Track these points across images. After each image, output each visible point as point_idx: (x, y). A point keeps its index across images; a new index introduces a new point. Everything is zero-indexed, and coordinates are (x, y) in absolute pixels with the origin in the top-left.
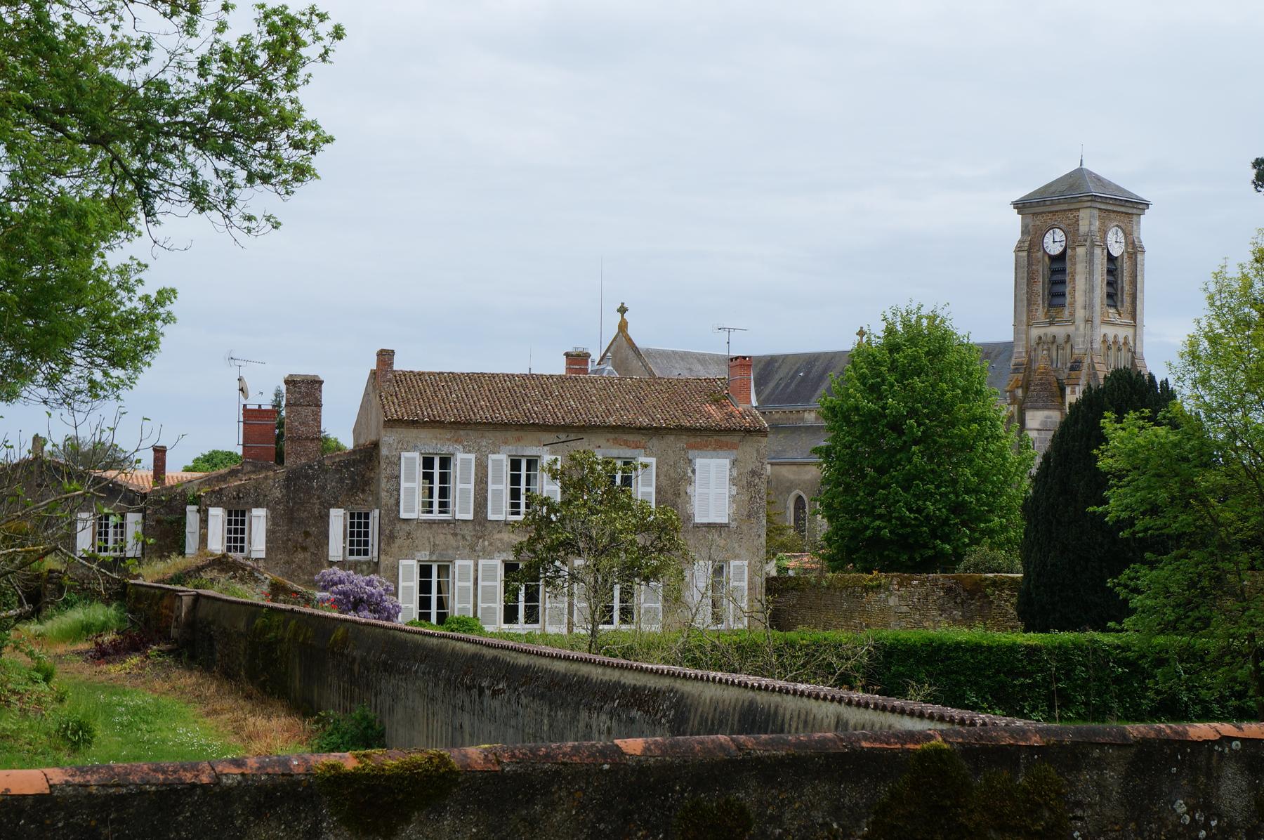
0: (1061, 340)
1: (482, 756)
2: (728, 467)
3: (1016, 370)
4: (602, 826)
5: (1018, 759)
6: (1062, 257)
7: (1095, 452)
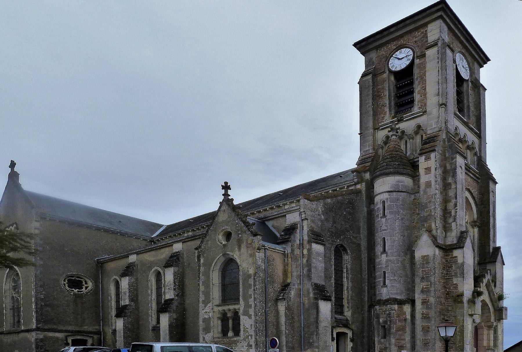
6: (408, 71)
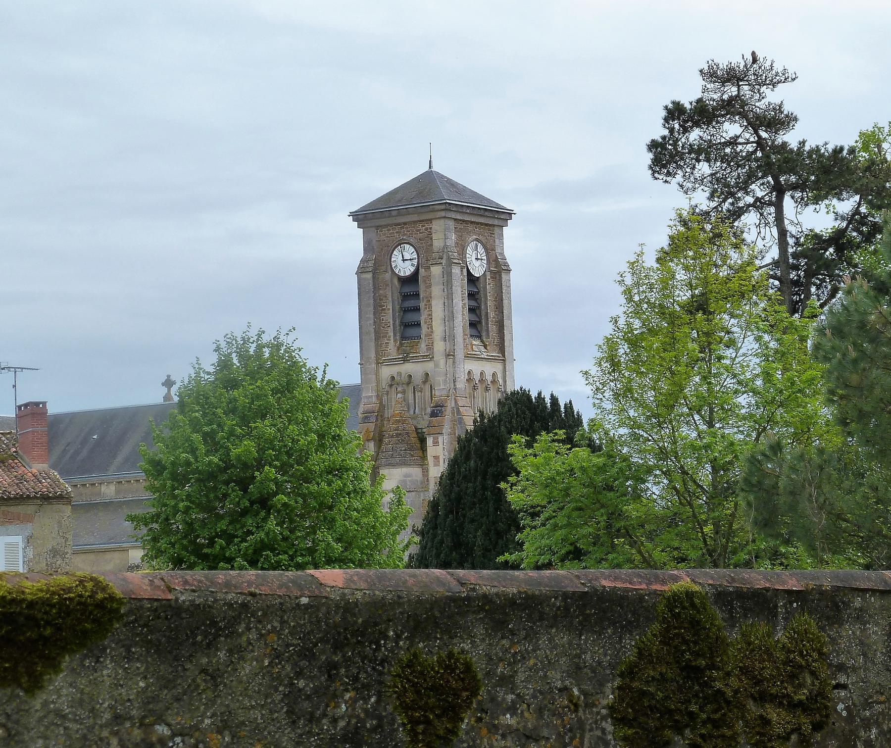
0: (418, 379)
1: (146, 581)
2: (21, 545)
3: (366, 419)
4: (301, 683)
5: (776, 607)
6: (413, 278)
7: (502, 485)
